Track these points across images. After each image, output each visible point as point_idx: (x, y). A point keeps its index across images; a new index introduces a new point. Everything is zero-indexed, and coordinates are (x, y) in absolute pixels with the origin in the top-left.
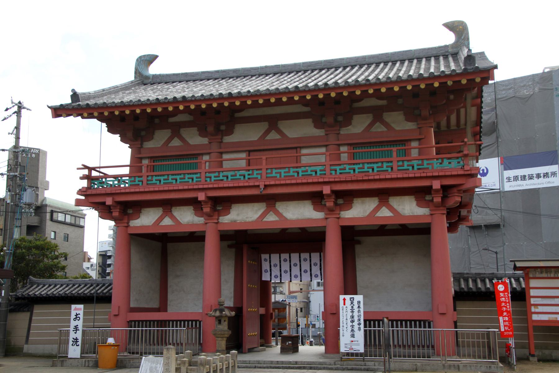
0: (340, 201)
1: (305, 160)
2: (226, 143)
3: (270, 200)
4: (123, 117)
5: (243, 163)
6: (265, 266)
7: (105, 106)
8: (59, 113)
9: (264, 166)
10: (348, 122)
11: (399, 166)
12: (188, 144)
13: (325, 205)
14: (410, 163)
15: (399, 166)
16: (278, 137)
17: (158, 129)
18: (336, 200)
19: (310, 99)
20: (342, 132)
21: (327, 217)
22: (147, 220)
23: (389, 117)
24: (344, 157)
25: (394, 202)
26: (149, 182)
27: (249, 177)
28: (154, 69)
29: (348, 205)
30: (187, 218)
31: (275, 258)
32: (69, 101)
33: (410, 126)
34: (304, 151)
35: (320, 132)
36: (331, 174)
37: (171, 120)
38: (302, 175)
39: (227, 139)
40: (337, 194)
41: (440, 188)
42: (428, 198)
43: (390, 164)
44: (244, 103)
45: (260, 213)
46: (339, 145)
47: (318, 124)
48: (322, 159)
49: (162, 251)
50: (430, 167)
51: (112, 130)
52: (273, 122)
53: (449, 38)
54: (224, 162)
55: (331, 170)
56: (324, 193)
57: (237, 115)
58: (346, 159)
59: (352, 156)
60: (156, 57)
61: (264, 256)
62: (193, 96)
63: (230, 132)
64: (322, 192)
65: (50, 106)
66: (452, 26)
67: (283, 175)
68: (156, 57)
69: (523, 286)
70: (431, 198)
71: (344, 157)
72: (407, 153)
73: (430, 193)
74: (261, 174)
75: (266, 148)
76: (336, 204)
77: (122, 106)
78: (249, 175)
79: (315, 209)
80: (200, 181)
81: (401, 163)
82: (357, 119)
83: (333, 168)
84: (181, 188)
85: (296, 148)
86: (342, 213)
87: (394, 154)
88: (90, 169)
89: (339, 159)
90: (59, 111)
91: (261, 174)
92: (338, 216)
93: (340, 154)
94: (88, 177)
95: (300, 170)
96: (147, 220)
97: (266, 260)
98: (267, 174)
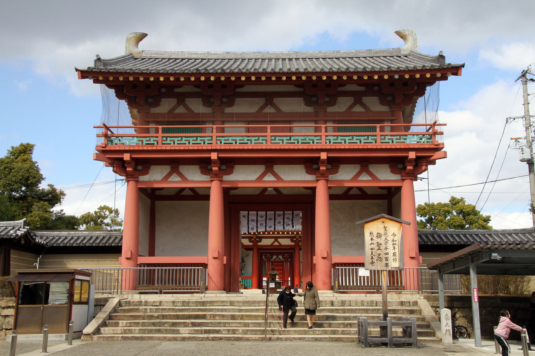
2: (226, 113)
4: (136, 84)
6: (243, 222)
7: (117, 74)
8: (86, 75)
9: (269, 133)
10: (157, 104)
11: (381, 139)
12: (192, 111)
13: (211, 170)
14: (342, 138)
15: (381, 139)
18: (136, 166)
19: (408, 79)
21: (403, 178)
22: (156, 177)
23: (366, 100)
26: (272, 142)
27: (241, 142)
30: (194, 178)
32: (92, 65)
33: (385, 109)
35: (309, 109)
36: (217, 143)
37: (177, 90)
40: (136, 162)
42: (315, 166)
44: (350, 78)
45: (164, 175)
47: (308, 103)
49: (152, 204)
51: (120, 95)
52: (269, 98)
55: (326, 140)
57: (238, 90)
60: (146, 35)
61: (243, 213)
62: (407, 67)
63: (231, 104)
65: (79, 68)
67: (145, 143)
68: (146, 35)
69: (499, 240)
70: (317, 167)
73: (317, 163)
74: (266, 140)
76: (135, 169)
77: (126, 74)
80: (321, 143)
82: (340, 99)
83: (218, 138)
86: (224, 176)
87: (269, 130)
88: (108, 128)
90: (84, 74)
91: (157, 141)
92: (136, 179)
94: (106, 136)
96: (156, 177)
97: (244, 216)
98: (162, 141)
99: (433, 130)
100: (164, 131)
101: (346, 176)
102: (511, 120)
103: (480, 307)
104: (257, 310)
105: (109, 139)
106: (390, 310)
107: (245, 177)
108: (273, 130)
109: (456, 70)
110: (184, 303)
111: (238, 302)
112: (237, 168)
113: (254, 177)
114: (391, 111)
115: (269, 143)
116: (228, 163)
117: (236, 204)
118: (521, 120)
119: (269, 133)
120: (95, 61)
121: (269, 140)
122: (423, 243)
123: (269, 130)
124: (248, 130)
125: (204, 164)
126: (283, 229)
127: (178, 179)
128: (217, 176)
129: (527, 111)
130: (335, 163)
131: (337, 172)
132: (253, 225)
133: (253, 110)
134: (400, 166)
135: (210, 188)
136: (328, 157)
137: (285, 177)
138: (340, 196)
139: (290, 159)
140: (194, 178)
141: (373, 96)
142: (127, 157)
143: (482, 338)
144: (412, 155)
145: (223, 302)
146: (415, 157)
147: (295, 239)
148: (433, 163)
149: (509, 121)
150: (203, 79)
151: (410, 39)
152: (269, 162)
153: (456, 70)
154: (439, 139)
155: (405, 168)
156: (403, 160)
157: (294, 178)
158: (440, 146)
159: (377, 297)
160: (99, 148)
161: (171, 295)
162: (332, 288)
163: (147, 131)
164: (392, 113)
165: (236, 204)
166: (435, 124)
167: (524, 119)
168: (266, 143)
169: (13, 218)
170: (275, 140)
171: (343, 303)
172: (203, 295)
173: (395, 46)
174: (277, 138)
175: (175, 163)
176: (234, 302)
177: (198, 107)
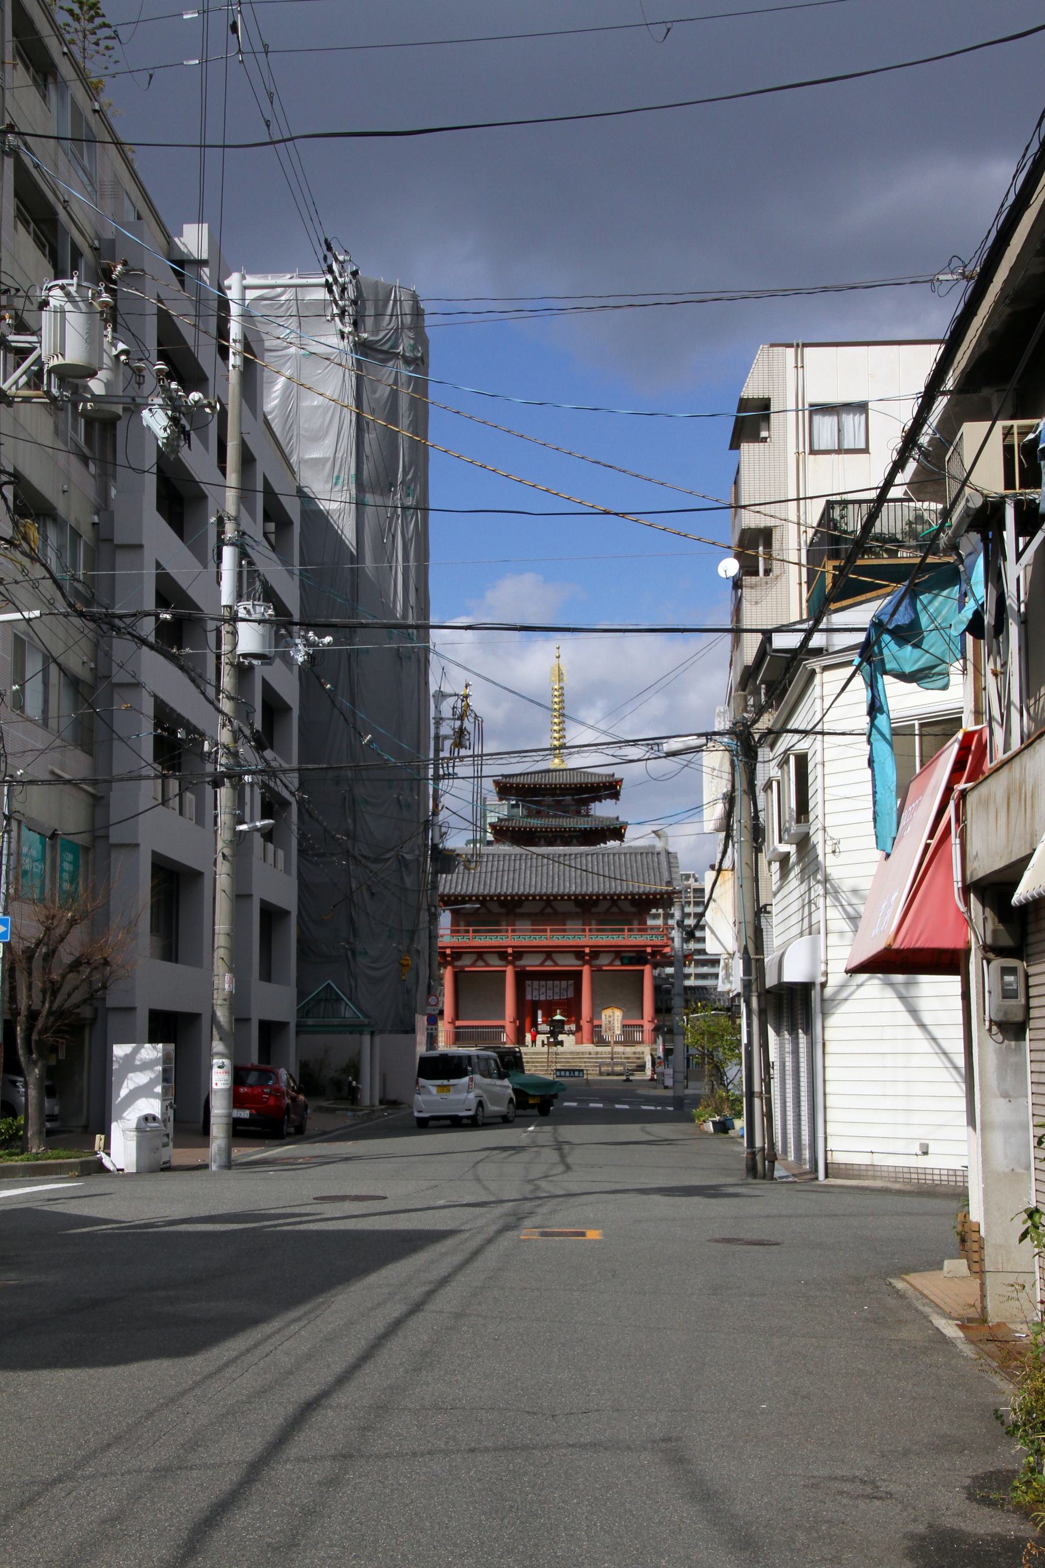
6: (528, 990)
31: (536, 983)
35: (578, 910)
39: (518, 911)
61: (528, 982)
107: (531, 963)
108: (552, 931)
112: (525, 955)
113: (538, 962)
116: (519, 953)
117: (522, 978)
124: (533, 931)
125: (502, 955)
126: (559, 991)
127: (482, 964)
128: (512, 963)
132: (536, 993)
133: (537, 910)
137: (560, 962)
139: (563, 950)
140: (495, 964)
142: (448, 951)
143: (261, 979)
152: (549, 953)
157: (567, 963)
159: (608, 1049)
162: (593, 1043)
163: (458, 931)
171: (597, 1053)
175: (480, 954)
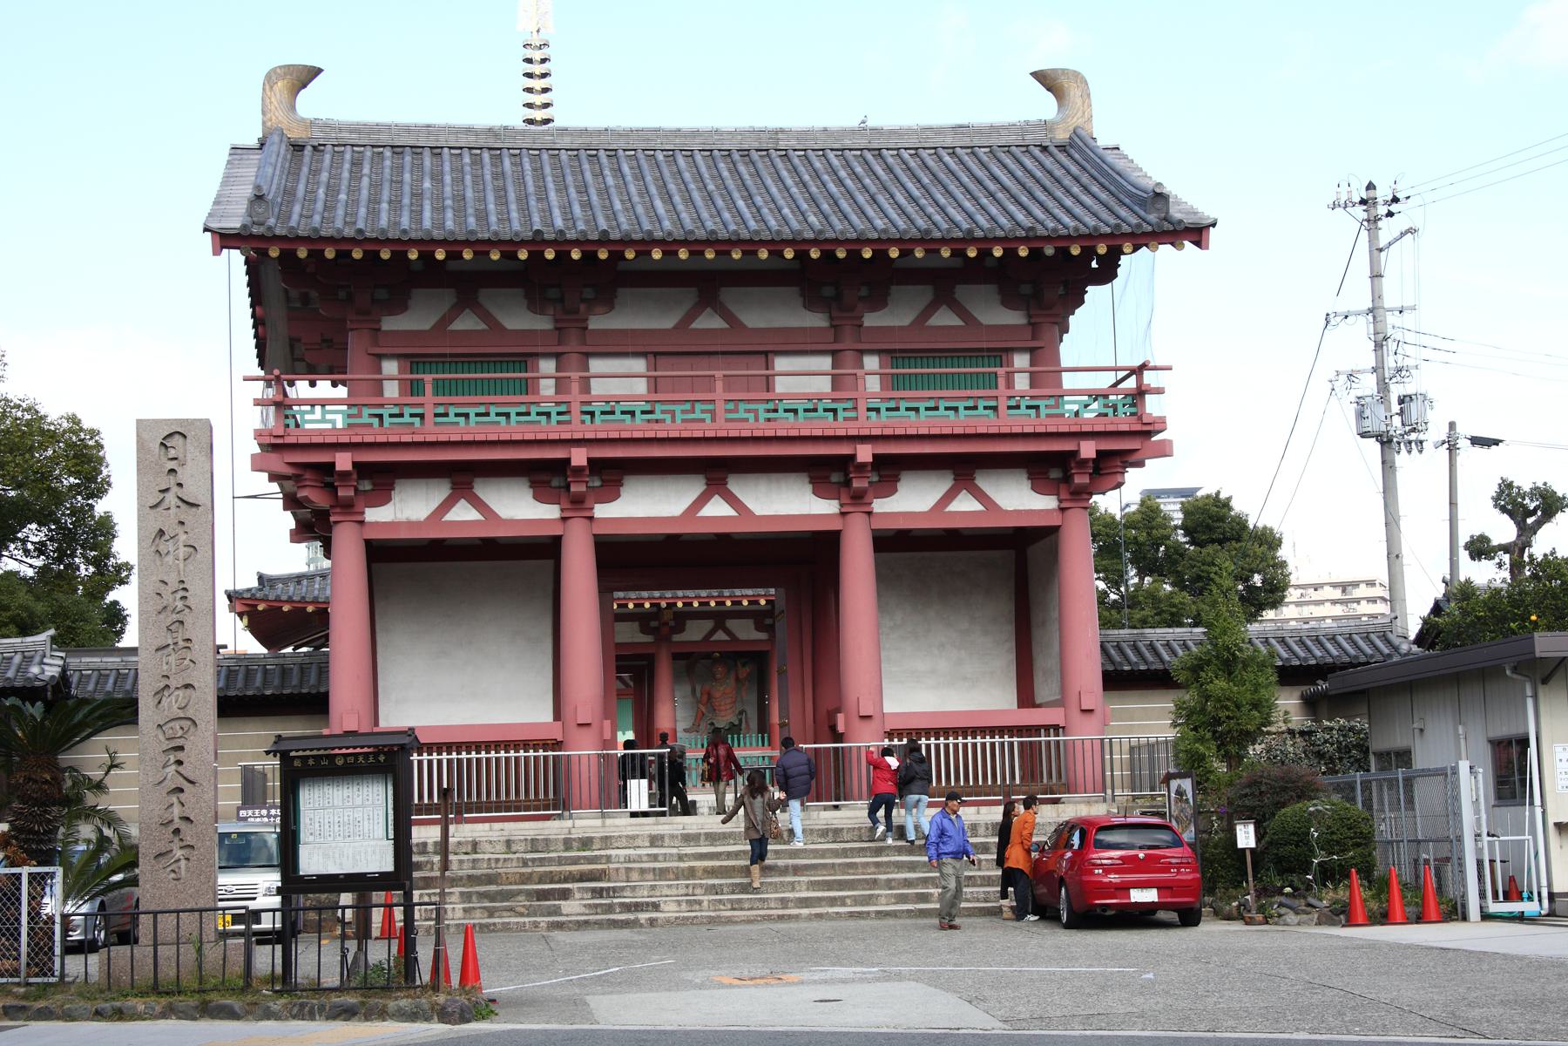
0: (366, 486)
1: (781, 385)
3: (715, 470)
5: (823, 385)
9: (719, 392)
16: (955, 321)
17: (966, 283)
20: (385, 327)
21: (1064, 505)
24: (391, 390)
25: (986, 483)
28: (314, 104)
29: (382, 495)
30: (518, 508)
34: (781, 364)
35: (817, 320)
36: (583, 422)
38: (559, 422)
41: (585, 463)
43: (710, 407)
46: (862, 352)
48: (640, 387)
50: (751, 416)
53: (1042, 107)
54: (593, 381)
56: (338, 468)
58: (396, 394)
59: (412, 388)
60: (319, 71)
64: (568, 460)
66: (1048, 80)
71: (391, 390)
72: (528, 387)
74: (713, 413)
75: (719, 349)
78: (559, 414)
79: (537, 497)
80: (569, 422)
81: (441, 410)
84: (393, 439)
85: (766, 353)
86: (368, 511)
89: (380, 393)
91: (422, 416)
93: (588, 378)
95: (385, 412)
99: (1136, 385)
100: (441, 388)
101: (914, 501)
102: (1339, 319)
103: (509, 1031)
104: (729, 855)
105: (288, 412)
106: (975, 845)
109: (1196, 233)
110: (534, 845)
111: (672, 837)
114: (1030, 324)
115: (720, 422)
118: (1362, 320)
119: (719, 392)
120: (251, 203)
121: (715, 411)
122: (1111, 668)
123: (429, 389)
129: (1377, 296)
130: (890, 469)
131: (893, 491)
134: (1055, 474)
135: (1465, 918)
136: (874, 456)
138: (894, 544)
140: (518, 508)
141: (985, 282)
142: (343, 461)
144: (1088, 450)
145: (634, 837)
146: (1094, 456)
147: (654, 624)
148: (1140, 464)
149: (1333, 322)
150: (550, 255)
151: (1074, 93)
153: (1196, 233)
154: (1152, 406)
155: (847, 483)
156: (1066, 461)
158: (1157, 427)
160: (267, 440)
161: (487, 825)
164: (1034, 328)
165: (623, 558)
166: (1144, 367)
167: (1370, 317)
168: (714, 420)
169: (25, 629)
170: (736, 411)
172: (569, 823)
173: (1033, 117)
174: (742, 406)
176: (662, 837)
177: (519, 319)
